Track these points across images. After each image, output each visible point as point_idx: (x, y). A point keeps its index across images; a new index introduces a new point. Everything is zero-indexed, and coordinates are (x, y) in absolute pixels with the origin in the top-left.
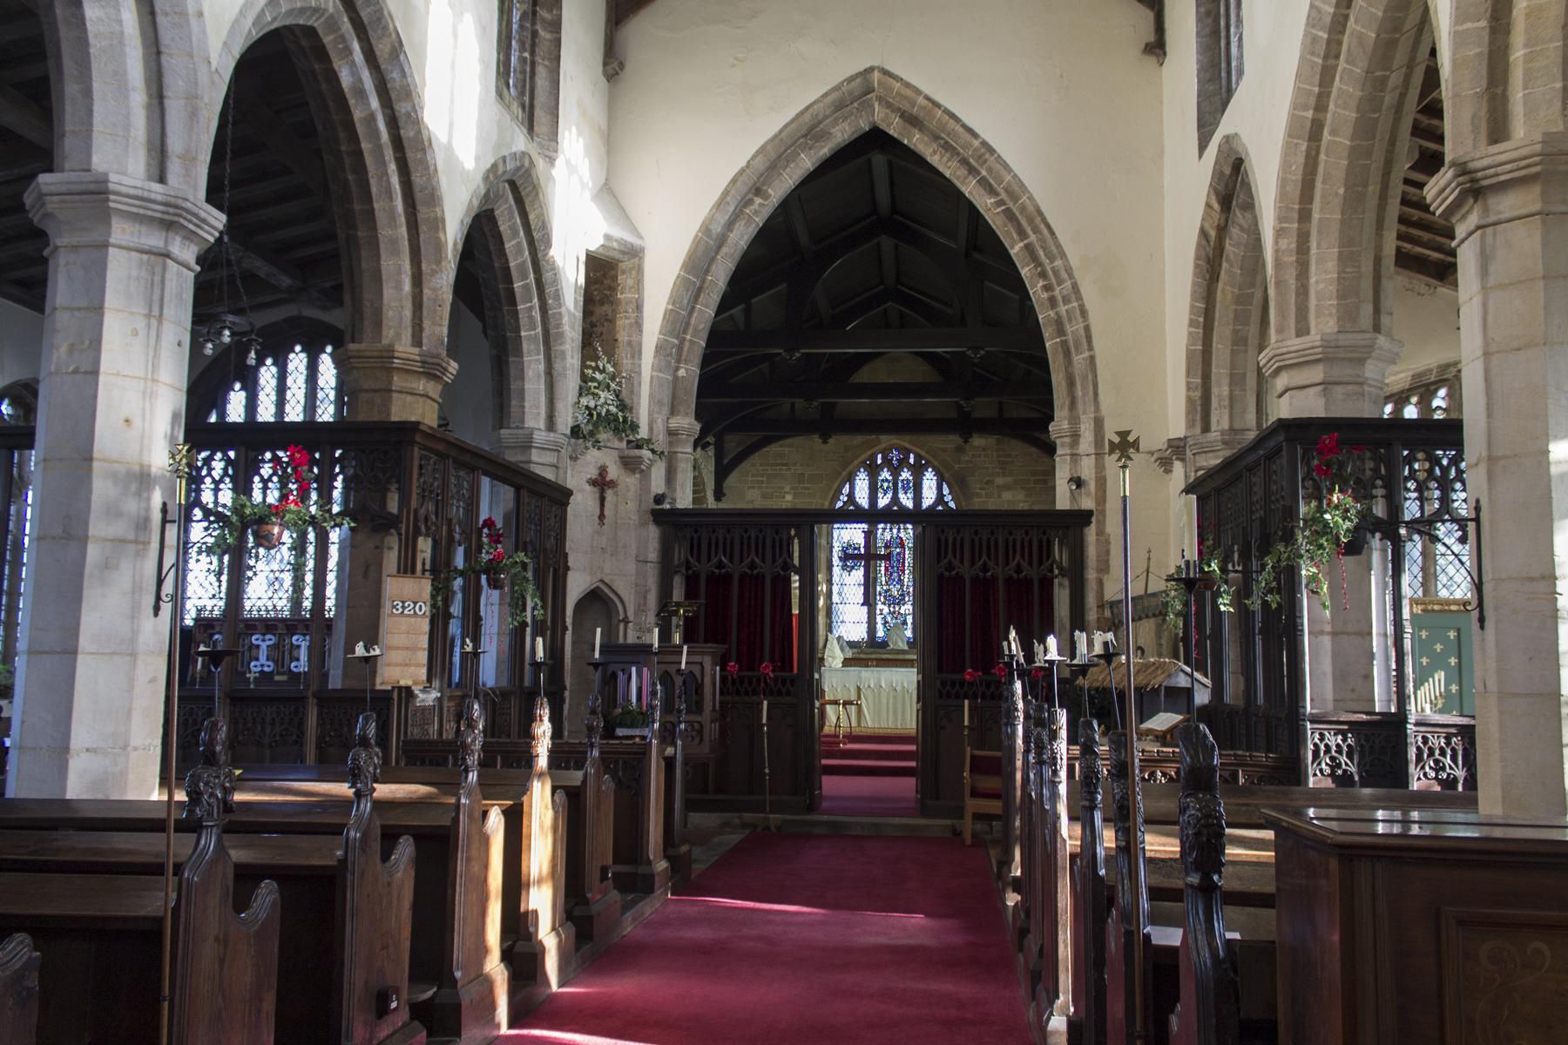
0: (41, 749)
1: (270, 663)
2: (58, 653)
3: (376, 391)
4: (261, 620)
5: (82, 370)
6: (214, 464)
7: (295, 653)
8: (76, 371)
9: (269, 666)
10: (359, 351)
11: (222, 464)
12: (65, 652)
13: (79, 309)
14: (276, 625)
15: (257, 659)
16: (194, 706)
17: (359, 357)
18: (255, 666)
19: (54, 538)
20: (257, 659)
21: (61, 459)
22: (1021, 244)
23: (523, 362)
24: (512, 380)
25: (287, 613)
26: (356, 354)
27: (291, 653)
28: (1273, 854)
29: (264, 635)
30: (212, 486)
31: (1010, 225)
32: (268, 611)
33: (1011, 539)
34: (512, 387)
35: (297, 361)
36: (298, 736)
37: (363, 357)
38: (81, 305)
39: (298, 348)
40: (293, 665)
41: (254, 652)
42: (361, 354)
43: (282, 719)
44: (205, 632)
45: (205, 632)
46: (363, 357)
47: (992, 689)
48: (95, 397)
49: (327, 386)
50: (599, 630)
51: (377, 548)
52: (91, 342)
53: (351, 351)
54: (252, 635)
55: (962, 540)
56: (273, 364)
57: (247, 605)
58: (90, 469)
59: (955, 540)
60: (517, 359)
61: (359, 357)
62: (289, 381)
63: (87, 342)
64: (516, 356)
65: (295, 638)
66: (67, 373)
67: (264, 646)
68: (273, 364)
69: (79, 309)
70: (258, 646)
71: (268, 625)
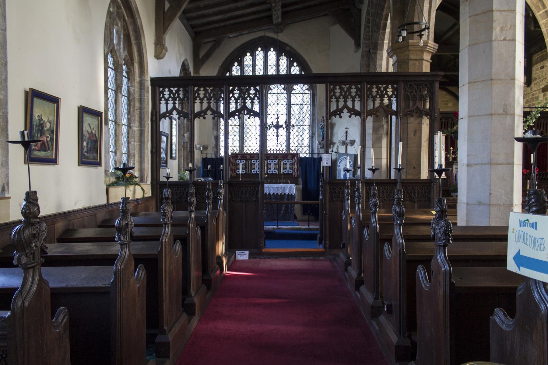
0: (500, 205)
1: (291, 170)
2: (505, 164)
3: (416, 60)
4: (273, 154)
5: (508, 39)
6: (352, 90)
7: (269, 166)
8: (505, 39)
9: (291, 171)
10: (413, 43)
11: (355, 90)
12: (508, 164)
13: (504, 11)
14: (270, 156)
15: (254, 169)
16: (342, 186)
17: (413, 46)
18: (254, 172)
19: (499, 114)
20: (254, 169)
21: (500, 79)
22: (544, 11)
23: (383, 53)
24: (377, 61)
25: (284, 152)
26: (412, 44)
27: (267, 166)
28: (265, 227)
29: (241, 160)
30: (250, 101)
31: (539, 3)
32: (249, 151)
33: (453, 122)
34: (377, 63)
35: (260, 55)
36: (256, 198)
37: (415, 46)
38: (506, 9)
39: (272, 49)
40: (268, 171)
41: (253, 166)
42: (414, 44)
43: (387, 191)
44: (234, 159)
45: (234, 159)
46: (415, 46)
47: (544, 176)
48: (515, 51)
49: (272, 64)
50: (532, 155)
51: (419, 123)
52: (511, 26)
53: (410, 43)
54: (252, 160)
55: (448, 122)
56: (250, 56)
57: (268, 149)
58: (514, 84)
59: (445, 122)
60: (380, 52)
61: (413, 46)
62: (257, 62)
63: (509, 26)
64: (380, 51)
65: (268, 161)
66: (500, 40)
67: (257, 164)
68: (250, 56)
69: (504, 11)
70: (254, 164)
71: (276, 156)
